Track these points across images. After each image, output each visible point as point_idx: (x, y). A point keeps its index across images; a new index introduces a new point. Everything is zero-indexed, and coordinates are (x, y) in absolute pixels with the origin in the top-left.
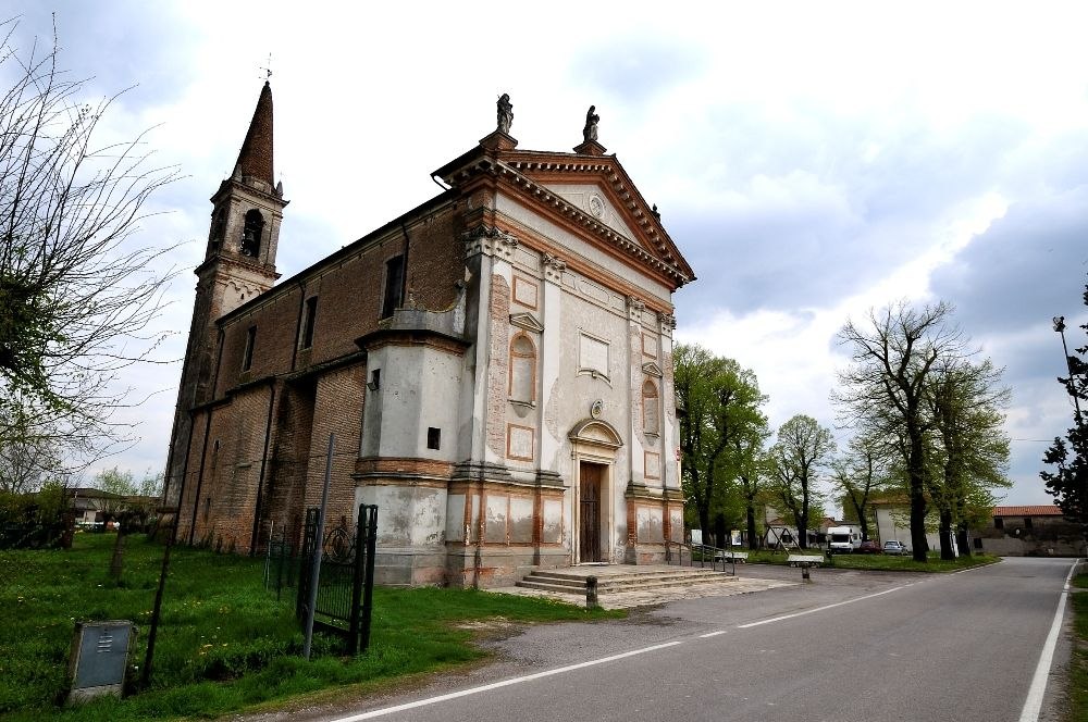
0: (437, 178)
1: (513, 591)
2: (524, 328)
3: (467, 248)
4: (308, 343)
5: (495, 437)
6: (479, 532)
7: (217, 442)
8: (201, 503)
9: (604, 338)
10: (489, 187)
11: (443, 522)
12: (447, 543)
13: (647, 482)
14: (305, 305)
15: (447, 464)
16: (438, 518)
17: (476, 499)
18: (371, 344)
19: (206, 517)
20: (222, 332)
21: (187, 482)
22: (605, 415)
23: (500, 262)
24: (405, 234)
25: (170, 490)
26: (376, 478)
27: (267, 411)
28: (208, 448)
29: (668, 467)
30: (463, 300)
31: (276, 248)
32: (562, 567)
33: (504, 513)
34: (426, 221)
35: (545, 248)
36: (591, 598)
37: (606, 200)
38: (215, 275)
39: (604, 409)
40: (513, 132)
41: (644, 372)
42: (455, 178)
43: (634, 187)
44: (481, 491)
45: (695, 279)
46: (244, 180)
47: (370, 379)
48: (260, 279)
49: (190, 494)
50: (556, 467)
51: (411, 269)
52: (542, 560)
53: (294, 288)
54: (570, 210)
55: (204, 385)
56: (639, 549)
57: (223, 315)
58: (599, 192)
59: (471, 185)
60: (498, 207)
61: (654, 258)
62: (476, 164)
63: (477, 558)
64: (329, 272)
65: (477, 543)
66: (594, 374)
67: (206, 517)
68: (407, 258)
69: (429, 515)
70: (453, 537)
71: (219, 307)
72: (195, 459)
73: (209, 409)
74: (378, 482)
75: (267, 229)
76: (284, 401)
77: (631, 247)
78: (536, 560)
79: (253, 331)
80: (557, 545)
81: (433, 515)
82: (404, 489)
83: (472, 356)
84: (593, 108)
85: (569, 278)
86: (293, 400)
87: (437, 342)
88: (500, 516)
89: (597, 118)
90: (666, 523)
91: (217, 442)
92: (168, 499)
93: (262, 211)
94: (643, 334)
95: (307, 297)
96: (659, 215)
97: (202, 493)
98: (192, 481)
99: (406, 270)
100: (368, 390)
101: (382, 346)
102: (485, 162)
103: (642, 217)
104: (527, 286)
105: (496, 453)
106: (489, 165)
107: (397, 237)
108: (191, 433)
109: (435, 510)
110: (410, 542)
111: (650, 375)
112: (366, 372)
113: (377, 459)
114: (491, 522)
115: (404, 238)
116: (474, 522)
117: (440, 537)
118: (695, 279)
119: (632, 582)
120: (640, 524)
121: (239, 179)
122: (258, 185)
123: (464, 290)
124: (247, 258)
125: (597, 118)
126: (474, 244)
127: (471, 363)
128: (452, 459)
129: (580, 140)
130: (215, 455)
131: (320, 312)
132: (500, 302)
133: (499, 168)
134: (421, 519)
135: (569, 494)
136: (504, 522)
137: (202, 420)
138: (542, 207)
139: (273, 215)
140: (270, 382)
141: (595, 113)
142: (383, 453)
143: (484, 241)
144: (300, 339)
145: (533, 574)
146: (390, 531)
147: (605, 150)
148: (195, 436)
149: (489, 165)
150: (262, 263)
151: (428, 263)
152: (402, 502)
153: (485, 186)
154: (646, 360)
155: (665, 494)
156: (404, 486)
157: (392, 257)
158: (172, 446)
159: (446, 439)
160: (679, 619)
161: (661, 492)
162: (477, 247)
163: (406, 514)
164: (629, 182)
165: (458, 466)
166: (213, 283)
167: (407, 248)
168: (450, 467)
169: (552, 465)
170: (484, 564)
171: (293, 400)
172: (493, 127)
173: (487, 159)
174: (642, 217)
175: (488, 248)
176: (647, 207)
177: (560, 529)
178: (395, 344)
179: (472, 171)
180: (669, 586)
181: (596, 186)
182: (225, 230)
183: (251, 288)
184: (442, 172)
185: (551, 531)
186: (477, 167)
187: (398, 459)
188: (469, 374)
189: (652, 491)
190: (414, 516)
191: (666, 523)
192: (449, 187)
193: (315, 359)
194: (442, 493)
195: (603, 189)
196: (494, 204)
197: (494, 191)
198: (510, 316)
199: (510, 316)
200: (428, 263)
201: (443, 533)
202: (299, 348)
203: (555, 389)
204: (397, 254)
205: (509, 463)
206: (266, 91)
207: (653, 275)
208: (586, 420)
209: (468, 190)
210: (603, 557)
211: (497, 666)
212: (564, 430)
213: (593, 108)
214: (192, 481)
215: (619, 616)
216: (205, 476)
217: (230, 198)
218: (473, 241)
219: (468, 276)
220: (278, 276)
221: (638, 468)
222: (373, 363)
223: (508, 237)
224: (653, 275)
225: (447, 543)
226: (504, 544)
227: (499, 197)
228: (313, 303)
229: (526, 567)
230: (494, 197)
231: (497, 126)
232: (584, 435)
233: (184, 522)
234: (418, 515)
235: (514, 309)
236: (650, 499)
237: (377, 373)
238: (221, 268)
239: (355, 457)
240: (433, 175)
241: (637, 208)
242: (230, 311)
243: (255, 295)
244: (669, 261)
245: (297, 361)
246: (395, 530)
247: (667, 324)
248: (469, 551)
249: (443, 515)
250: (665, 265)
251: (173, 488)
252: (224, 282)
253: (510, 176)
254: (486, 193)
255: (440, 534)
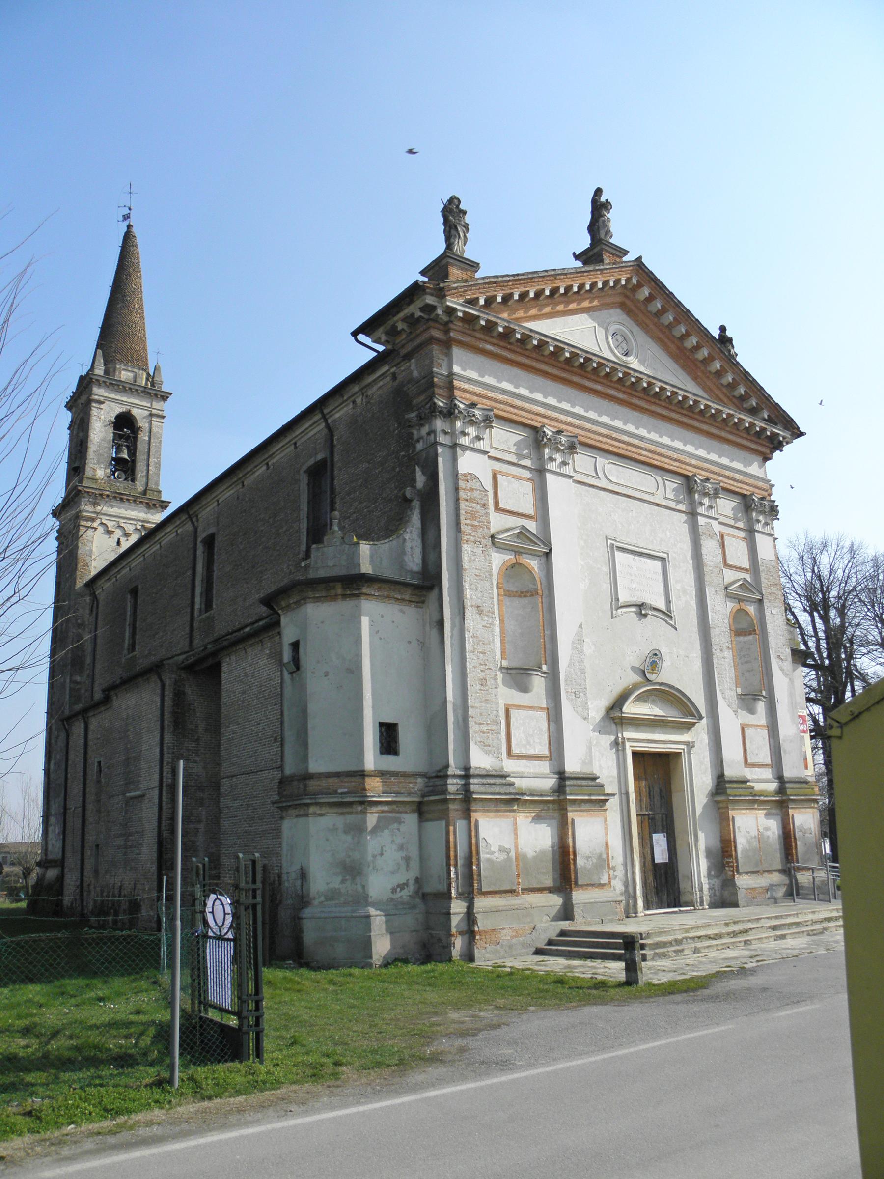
0: (361, 337)
1: (531, 962)
2: (518, 552)
3: (416, 437)
4: (208, 605)
5: (485, 728)
6: (470, 877)
7: (99, 763)
8: (88, 853)
9: (655, 548)
10: (438, 341)
11: (415, 864)
12: (424, 897)
13: (749, 773)
14: (200, 549)
15: (414, 775)
16: (407, 859)
17: (460, 825)
18: (283, 604)
19: (96, 872)
20: (95, 598)
21: (69, 824)
22: (667, 675)
23: (468, 453)
24: (328, 426)
25: (51, 835)
26: (308, 805)
27: (158, 713)
28: (89, 772)
29: (785, 746)
30: (415, 519)
31: (158, 464)
32: (611, 921)
33: (508, 844)
34: (354, 402)
35: (540, 419)
36: (632, 968)
37: (636, 330)
38: (77, 517)
39: (666, 664)
40: (470, 252)
41: (730, 596)
42: (387, 333)
43: (679, 304)
44: (467, 814)
45: (802, 434)
46: (107, 372)
47: (287, 656)
48: (138, 513)
49: (74, 839)
50: (591, 763)
51: (341, 477)
52: (577, 911)
53: (183, 524)
54: (574, 355)
55: (78, 679)
56: (742, 881)
57: (94, 573)
58: (623, 317)
59: (411, 340)
60: (456, 369)
61: (726, 411)
62: (414, 309)
63: (470, 917)
64: (226, 494)
65: (469, 896)
66: (641, 609)
67: (96, 872)
68: (332, 461)
69: (392, 856)
70: (433, 886)
71: (88, 559)
72: (75, 789)
73: (84, 713)
74: (312, 809)
75: (143, 437)
76: (179, 695)
77: (696, 402)
78: (567, 913)
79: (134, 592)
80: (601, 886)
81: (398, 855)
82: (350, 819)
83: (436, 604)
84: (598, 192)
85: (582, 461)
86: (191, 692)
87: (380, 589)
88: (502, 850)
89: (607, 206)
90: (788, 837)
91: (99, 763)
92: (50, 847)
93: (135, 412)
94: (722, 537)
95: (202, 536)
96: (730, 340)
97: (87, 837)
98: (74, 822)
99: (332, 479)
100: (286, 673)
101: (298, 604)
102: (428, 305)
103: (697, 347)
104: (516, 484)
105: (487, 753)
106: (434, 308)
107: (315, 429)
108: (67, 753)
109: (401, 848)
110: (366, 897)
111: (739, 600)
112: (280, 644)
113: (307, 777)
114: (489, 860)
115: (326, 431)
116: (460, 862)
117: (412, 887)
118: (802, 434)
119: (719, 936)
120: (741, 842)
121: (100, 371)
122: (125, 375)
123: (416, 504)
124: (121, 486)
125: (607, 206)
126: (425, 430)
127: (436, 617)
128: (422, 768)
129: (584, 242)
130: (99, 781)
131: (220, 556)
132: (473, 515)
133: (451, 311)
134: (380, 861)
135: (613, 804)
136: (509, 859)
137: (78, 728)
138: (528, 357)
139: (151, 415)
140: (156, 669)
141: (603, 199)
142: (315, 766)
143: (439, 424)
144: (198, 600)
145: (563, 933)
146: (336, 883)
147: (625, 253)
148: (72, 756)
149: (434, 308)
150: (141, 488)
151: (365, 465)
152: (349, 838)
153: (432, 340)
154: (730, 576)
155: (781, 790)
156: (350, 813)
157: (311, 462)
158: (47, 771)
159: (407, 738)
160: (765, 990)
161: (773, 786)
162: (429, 434)
163: (357, 855)
164: (669, 297)
165: (429, 778)
166: (77, 527)
167: (332, 446)
168: (419, 780)
169: (584, 763)
170: (482, 924)
171: (191, 692)
172: (440, 247)
173: (430, 300)
174: (697, 347)
175: (446, 433)
176: (705, 333)
177: (603, 862)
178: (318, 600)
179: (412, 321)
180: (783, 937)
181: (618, 310)
182: (87, 447)
183: (130, 528)
184: (367, 328)
185: (589, 865)
186: (418, 314)
187: (337, 775)
188: (434, 632)
189: (758, 787)
190: (370, 858)
191: (788, 837)
192: (381, 348)
193: (221, 628)
194: (411, 820)
195: (629, 312)
196: (450, 367)
197: (447, 345)
198: (493, 537)
199: (493, 537)
200: (365, 465)
201: (417, 880)
202: (196, 613)
203: (579, 641)
204: (320, 457)
205: (510, 766)
206: (128, 237)
207: (731, 437)
208: (636, 687)
209: (409, 347)
210: (683, 899)
211: (435, 1071)
212: (597, 707)
213: (598, 192)
214: (74, 822)
215: (670, 989)
216: (89, 813)
217: (89, 401)
218: (422, 425)
219: (421, 480)
220: (164, 505)
221: (732, 752)
222: (289, 632)
223: (477, 412)
224: (731, 437)
225: (424, 897)
226: (512, 892)
227: (456, 351)
228: (210, 542)
229: (550, 929)
230: (449, 355)
231: (444, 246)
232: (631, 709)
233: (71, 881)
234: (374, 856)
235: (497, 522)
236: (755, 800)
237: (295, 646)
238: (86, 508)
239: (277, 775)
240: (355, 334)
241: (687, 335)
242: (104, 564)
243: (134, 538)
244: (753, 411)
245: (196, 634)
246: (343, 881)
247: (762, 512)
248: (458, 907)
249: (414, 852)
250: (748, 420)
251: (54, 831)
252: (89, 524)
253: (470, 320)
254: (436, 350)
255: (411, 882)
